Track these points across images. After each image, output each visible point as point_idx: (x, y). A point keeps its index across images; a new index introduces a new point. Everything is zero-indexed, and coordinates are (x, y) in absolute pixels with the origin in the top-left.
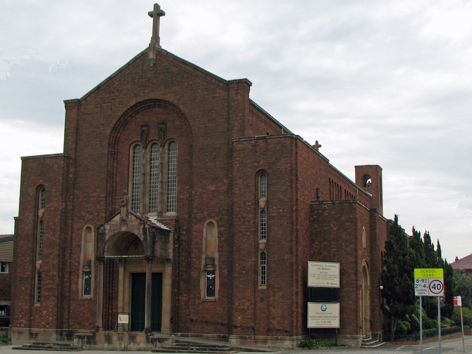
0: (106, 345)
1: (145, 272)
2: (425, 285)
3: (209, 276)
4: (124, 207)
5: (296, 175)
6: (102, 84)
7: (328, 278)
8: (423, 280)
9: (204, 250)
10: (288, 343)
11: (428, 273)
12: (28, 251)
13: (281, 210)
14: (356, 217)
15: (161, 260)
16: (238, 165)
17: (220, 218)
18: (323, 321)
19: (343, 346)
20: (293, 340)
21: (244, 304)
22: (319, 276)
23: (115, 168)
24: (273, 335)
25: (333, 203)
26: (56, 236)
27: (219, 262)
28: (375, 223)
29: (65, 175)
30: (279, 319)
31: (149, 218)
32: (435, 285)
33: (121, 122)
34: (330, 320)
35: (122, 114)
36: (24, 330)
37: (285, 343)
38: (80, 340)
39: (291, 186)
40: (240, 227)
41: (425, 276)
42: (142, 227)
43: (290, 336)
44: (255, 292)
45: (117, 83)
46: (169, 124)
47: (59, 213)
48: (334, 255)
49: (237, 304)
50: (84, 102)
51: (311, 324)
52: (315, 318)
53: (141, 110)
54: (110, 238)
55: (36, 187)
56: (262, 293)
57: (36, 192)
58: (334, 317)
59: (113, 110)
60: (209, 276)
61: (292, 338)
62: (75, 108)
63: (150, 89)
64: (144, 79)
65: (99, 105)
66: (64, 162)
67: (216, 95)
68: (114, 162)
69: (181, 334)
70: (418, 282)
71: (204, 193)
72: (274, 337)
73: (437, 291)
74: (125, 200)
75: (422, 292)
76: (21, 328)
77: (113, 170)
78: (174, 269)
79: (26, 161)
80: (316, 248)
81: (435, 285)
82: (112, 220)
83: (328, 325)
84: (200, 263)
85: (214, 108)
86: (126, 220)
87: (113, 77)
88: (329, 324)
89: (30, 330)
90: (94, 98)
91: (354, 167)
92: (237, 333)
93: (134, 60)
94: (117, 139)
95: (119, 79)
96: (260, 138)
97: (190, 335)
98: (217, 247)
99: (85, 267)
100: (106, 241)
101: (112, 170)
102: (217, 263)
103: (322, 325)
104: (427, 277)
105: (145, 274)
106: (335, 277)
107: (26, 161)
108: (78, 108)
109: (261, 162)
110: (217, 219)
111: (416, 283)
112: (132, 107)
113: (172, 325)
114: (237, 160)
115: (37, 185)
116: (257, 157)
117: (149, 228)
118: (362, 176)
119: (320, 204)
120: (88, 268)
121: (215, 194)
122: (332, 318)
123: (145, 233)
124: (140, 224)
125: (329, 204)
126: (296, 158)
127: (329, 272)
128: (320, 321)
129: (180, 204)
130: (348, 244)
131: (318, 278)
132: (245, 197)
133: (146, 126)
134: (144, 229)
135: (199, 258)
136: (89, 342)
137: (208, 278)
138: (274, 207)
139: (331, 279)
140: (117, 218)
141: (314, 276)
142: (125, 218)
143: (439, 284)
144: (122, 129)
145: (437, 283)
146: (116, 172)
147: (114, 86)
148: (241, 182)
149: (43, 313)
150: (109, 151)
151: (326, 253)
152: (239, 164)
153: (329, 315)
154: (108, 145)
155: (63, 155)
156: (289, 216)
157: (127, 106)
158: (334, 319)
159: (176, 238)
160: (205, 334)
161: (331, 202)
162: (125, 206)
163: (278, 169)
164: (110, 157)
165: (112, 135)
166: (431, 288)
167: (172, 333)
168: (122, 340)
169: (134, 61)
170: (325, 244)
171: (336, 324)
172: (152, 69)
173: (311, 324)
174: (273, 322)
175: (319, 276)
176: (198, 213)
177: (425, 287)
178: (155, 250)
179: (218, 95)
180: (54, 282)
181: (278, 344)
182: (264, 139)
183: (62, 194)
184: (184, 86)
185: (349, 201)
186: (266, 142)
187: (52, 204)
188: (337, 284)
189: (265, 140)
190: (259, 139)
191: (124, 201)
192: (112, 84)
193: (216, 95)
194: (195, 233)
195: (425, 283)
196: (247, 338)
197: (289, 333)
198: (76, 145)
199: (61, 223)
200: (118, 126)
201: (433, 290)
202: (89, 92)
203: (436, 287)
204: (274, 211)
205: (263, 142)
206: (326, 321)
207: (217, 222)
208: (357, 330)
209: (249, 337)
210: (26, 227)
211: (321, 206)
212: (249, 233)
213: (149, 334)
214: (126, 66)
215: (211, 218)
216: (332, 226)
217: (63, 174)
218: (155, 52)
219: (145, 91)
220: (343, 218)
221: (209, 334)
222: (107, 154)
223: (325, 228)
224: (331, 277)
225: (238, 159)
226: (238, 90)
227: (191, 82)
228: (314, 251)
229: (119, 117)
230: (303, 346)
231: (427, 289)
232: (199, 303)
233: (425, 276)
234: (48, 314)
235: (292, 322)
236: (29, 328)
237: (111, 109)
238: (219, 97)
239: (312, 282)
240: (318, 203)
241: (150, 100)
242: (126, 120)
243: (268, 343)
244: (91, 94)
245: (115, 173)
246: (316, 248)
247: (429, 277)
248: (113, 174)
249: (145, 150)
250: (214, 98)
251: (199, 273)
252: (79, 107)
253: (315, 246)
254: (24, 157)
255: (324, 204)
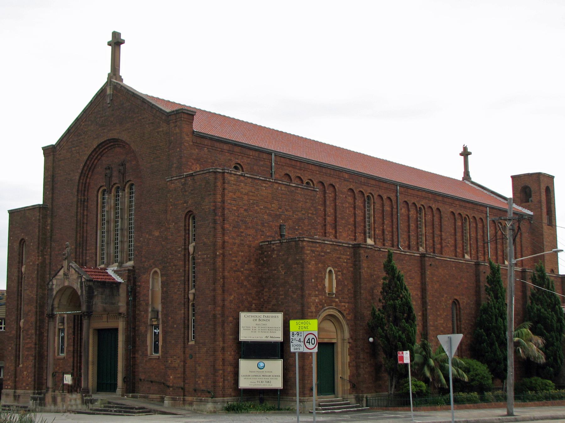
0: (53, 407)
1: (117, 327)
2: (300, 339)
3: (155, 331)
4: (65, 260)
5: (223, 214)
6: (71, 127)
7: (267, 331)
8: (298, 333)
9: (150, 303)
10: (210, 406)
11: (303, 325)
12: (14, 310)
13: (205, 256)
14: (303, 258)
15: (115, 315)
16: (171, 207)
17: (163, 266)
18: (260, 380)
19: (291, 411)
20: (215, 402)
21: (175, 361)
22: (255, 329)
23: (85, 217)
24: (198, 397)
25: (280, 242)
26: (34, 292)
27: (162, 315)
28: (359, 261)
29: (41, 227)
30: (203, 378)
31: (107, 270)
32: (309, 339)
33: (88, 166)
34: (269, 380)
35: (87, 157)
36: (10, 392)
37: (208, 405)
38: (34, 402)
39: (214, 228)
40: (172, 276)
41: (300, 328)
42: (80, 280)
43: (212, 398)
44: (184, 347)
45: (83, 124)
46: (128, 165)
47: (36, 267)
48: (282, 303)
49: (170, 362)
50: (58, 148)
51: (244, 384)
52: (249, 377)
53: (104, 152)
54: (57, 293)
55: (19, 241)
56: (191, 350)
57: (20, 246)
58: (275, 376)
59: (81, 153)
60: (155, 331)
61: (215, 400)
62: (51, 155)
63: (109, 128)
64: (104, 118)
65: (70, 150)
66: (39, 213)
67: (160, 130)
68: (84, 210)
69: (132, 396)
70: (293, 335)
71: (150, 239)
72: (199, 398)
73: (311, 346)
74: (66, 252)
75: (298, 347)
76: (8, 390)
77: (83, 218)
78: (128, 323)
79: (13, 213)
80: (266, 296)
81: (309, 339)
82: (58, 274)
83: (261, 385)
84: (147, 316)
85: (158, 144)
86: (68, 274)
87: (80, 118)
88: (268, 384)
89: (15, 392)
90: (66, 142)
91: (510, 177)
92: (170, 394)
93: (95, 97)
94: (87, 184)
95: (85, 119)
96: (189, 175)
97: (139, 396)
98: (161, 298)
99: (153, 320)
100: (54, 296)
101: (82, 218)
102: (160, 316)
103: (258, 385)
104: (302, 330)
105: (116, 330)
106: (277, 329)
107: (13, 213)
108: (53, 154)
109: (190, 202)
110: (160, 267)
111: (291, 337)
112: (95, 149)
113: (125, 385)
114: (171, 202)
115: (20, 239)
116: (186, 197)
117: (84, 282)
118: (520, 188)
119: (269, 244)
120: (62, 325)
121: (159, 240)
122: (272, 377)
123: (81, 287)
124: (78, 278)
125: (277, 244)
126: (223, 195)
127: (269, 324)
128: (256, 381)
129: (136, 252)
130: (294, 290)
131: (253, 331)
132: (177, 242)
133: (109, 169)
134: (81, 283)
135: (146, 311)
136: (40, 404)
137: (155, 333)
138: (200, 253)
139: (270, 332)
140: (61, 272)
141: (248, 328)
142: (66, 272)
143: (313, 338)
144: (90, 173)
145: (311, 337)
146: (87, 221)
147: (82, 127)
148: (172, 226)
149: (24, 374)
150: (78, 199)
151: (274, 302)
152: (172, 205)
153: (268, 374)
154: (77, 193)
155: (41, 206)
156: (212, 261)
157: (91, 149)
158: (275, 379)
159: (130, 290)
160: (151, 395)
161: (278, 242)
162: (66, 259)
163: (203, 209)
164: (79, 205)
165: (81, 181)
166: (306, 342)
167: (125, 394)
168: (64, 401)
169: (96, 98)
170: (274, 291)
171: (278, 384)
172: (109, 105)
173: (244, 384)
174: (199, 382)
175: (255, 329)
176: (145, 262)
177: (300, 341)
178: (92, 305)
179: (161, 129)
180: (32, 341)
181: (202, 407)
182: (192, 176)
183: (38, 247)
184: (135, 122)
185: (295, 240)
186: (194, 179)
187: (30, 258)
188: (280, 338)
189: (193, 177)
190: (188, 177)
191: (65, 254)
192: (79, 126)
193: (160, 130)
194: (143, 284)
195: (300, 337)
196: (177, 400)
197: (212, 393)
198: (53, 194)
199: (38, 279)
200: (86, 171)
201: (307, 345)
202: (62, 137)
203: (310, 341)
204: (199, 257)
205: (191, 180)
206: (264, 380)
207: (160, 270)
208: (306, 391)
209: (178, 399)
210: (12, 284)
211: (270, 247)
212: (179, 283)
213: (84, 395)
214: (89, 105)
215: (156, 266)
216: (280, 269)
217: (39, 227)
218: (112, 86)
219: (105, 131)
220: (290, 260)
221: (154, 395)
222: (76, 202)
223: (274, 272)
224: (271, 329)
225: (171, 200)
226: (176, 122)
227: (140, 118)
228: (264, 300)
229: (85, 161)
230: (231, 409)
231: (302, 344)
232: (146, 361)
233: (300, 328)
234: (28, 375)
235: (215, 382)
236: (14, 390)
237: (79, 153)
238: (163, 131)
239: (245, 336)
240: (267, 243)
241: (110, 141)
242: (93, 163)
243: (194, 406)
244: (63, 138)
245: (85, 222)
246: (266, 296)
247: (303, 330)
248: (83, 223)
249: (109, 195)
250: (158, 132)
251: (146, 328)
252: (55, 153)
253: (265, 294)
254: (11, 210)
255: (273, 244)
